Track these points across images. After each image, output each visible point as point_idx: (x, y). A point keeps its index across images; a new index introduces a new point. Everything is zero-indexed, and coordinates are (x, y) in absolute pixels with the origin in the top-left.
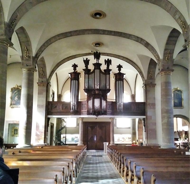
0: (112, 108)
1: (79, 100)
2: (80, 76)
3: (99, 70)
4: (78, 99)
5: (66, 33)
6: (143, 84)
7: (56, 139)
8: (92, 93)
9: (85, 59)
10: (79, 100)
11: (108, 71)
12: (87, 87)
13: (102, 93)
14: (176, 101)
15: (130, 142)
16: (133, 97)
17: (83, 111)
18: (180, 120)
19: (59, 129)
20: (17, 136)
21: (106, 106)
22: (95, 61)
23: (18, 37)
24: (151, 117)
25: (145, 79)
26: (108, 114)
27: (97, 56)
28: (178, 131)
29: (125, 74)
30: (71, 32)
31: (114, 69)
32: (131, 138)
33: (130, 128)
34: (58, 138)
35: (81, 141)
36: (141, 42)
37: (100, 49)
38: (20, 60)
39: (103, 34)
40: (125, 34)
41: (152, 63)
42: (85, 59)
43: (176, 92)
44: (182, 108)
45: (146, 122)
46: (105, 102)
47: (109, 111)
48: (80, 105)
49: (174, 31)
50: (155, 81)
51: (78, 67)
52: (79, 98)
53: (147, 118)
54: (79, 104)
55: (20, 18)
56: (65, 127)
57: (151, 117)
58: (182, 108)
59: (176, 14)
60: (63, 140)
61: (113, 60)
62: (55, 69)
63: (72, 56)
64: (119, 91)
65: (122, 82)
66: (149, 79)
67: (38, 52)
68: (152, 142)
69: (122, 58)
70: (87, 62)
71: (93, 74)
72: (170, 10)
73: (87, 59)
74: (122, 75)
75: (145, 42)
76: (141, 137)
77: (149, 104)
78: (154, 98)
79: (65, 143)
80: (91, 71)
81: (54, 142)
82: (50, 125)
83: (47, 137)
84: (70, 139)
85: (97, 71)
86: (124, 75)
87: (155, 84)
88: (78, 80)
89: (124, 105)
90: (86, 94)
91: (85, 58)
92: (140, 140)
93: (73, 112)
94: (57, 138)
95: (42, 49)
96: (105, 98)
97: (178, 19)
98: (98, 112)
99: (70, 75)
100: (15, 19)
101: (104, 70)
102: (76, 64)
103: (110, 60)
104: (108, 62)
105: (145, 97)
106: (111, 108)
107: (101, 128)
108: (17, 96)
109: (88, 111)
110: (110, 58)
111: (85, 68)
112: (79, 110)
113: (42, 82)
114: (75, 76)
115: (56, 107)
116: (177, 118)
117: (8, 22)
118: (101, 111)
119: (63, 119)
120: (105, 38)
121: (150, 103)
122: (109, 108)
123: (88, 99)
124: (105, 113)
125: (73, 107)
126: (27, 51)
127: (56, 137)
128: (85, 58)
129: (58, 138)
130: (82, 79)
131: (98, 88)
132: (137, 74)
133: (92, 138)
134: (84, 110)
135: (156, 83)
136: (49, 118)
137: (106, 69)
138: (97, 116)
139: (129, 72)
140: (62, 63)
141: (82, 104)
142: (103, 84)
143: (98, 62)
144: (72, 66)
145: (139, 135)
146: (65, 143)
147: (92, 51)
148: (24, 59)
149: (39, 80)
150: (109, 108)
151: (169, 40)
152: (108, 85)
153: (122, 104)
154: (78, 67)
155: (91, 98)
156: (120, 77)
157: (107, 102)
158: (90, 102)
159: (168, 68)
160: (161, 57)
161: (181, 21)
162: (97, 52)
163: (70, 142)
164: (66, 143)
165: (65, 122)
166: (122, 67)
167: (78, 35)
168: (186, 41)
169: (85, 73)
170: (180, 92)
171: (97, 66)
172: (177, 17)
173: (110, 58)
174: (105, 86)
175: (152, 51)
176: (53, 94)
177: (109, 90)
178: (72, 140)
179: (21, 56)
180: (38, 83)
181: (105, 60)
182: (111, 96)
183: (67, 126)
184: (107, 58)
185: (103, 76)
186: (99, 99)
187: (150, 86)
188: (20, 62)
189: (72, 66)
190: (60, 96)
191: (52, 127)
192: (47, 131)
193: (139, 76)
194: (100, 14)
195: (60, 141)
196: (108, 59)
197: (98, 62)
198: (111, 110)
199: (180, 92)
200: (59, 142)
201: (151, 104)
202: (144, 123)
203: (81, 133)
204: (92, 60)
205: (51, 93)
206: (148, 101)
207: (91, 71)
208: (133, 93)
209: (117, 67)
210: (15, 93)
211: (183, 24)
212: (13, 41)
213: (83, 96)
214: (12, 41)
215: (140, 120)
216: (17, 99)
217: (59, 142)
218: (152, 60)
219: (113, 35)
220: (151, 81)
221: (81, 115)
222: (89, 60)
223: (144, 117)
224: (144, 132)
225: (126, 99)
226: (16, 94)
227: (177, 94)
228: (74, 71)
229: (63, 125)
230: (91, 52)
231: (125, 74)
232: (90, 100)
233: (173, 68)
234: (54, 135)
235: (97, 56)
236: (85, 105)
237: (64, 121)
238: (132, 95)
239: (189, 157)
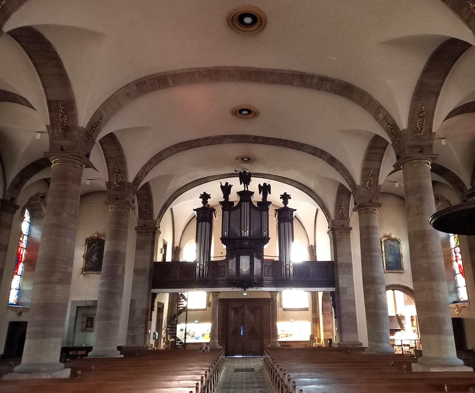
0: (272, 272)
1: (212, 259)
2: (214, 215)
3: (248, 203)
4: (210, 257)
5: (190, 142)
6: (329, 228)
7: (167, 334)
9: (224, 185)
10: (212, 259)
11: (264, 205)
13: (256, 244)
14: (390, 259)
16: (312, 250)
18: (400, 295)
19: (174, 314)
20: (90, 331)
21: (262, 269)
22: (241, 188)
23: (103, 150)
24: (345, 289)
25: (332, 219)
26: (266, 284)
27: (245, 178)
28: (397, 315)
29: (295, 210)
30: (198, 140)
31: (275, 197)
33: (307, 309)
34: (171, 332)
36: (321, 155)
37: (249, 168)
38: (103, 186)
39: (256, 142)
40: (292, 142)
41: (342, 193)
42: (224, 185)
43: (389, 241)
44: (402, 271)
45: (336, 299)
47: (267, 279)
49: (376, 138)
50: (348, 223)
51: (210, 198)
52: (212, 254)
55: (107, 120)
56: (185, 309)
57: (345, 289)
58: (402, 271)
59: (379, 112)
60: (180, 335)
61: (273, 184)
62: (169, 203)
63: (200, 179)
64: (285, 238)
65: (290, 224)
66: (338, 219)
67: (140, 175)
68: (348, 339)
69: (289, 182)
70: (226, 189)
71: (238, 211)
72: (368, 105)
73: (227, 183)
74: (289, 212)
75: (329, 156)
76: (329, 327)
78: (350, 254)
79: (185, 341)
80: (235, 205)
81: (162, 340)
82: (156, 308)
83: (150, 331)
85: (246, 205)
86: (294, 212)
87: (351, 229)
88: (210, 221)
89: (296, 267)
90: (225, 247)
91: (223, 182)
94: (168, 332)
95: (147, 170)
96: (260, 254)
97: (382, 120)
99: (195, 212)
100: (99, 122)
101: (259, 203)
102: (208, 193)
103: (267, 184)
104: (265, 189)
105: (333, 254)
106: (270, 272)
107: (253, 310)
108: (96, 253)
110: (267, 181)
111: (223, 200)
113: (145, 226)
114: (204, 215)
116: (393, 290)
117: (85, 128)
119: (182, 295)
120: (259, 150)
121: (343, 263)
122: (267, 274)
124: (260, 283)
126: (119, 173)
127: (168, 329)
128: (223, 182)
129: (171, 332)
130: (217, 220)
131: (248, 235)
132: (317, 209)
133: (237, 331)
136: (155, 293)
137: (261, 200)
139: (303, 206)
142: (256, 228)
143: (246, 189)
144: (200, 198)
145: (324, 325)
146: (184, 342)
147: (235, 171)
148: (113, 187)
149: (138, 222)
150: (267, 274)
151: (370, 153)
153: (291, 265)
154: (210, 198)
156: (286, 215)
157: (263, 261)
158: (232, 262)
159: (370, 201)
160: (358, 181)
161: (388, 124)
162: (245, 172)
164: (187, 342)
165: (186, 300)
166: (290, 198)
167: (211, 144)
168: (398, 157)
169: (222, 209)
170: (396, 242)
171: (245, 195)
172: (381, 116)
173: (267, 181)
175: (341, 172)
176: (165, 246)
177: (266, 240)
179: (106, 183)
180: (136, 229)
181: (260, 184)
182: (271, 250)
183: (189, 307)
184: (262, 181)
185: (256, 214)
186: (248, 257)
187: (341, 232)
188: (105, 190)
189: (200, 198)
190: (177, 251)
191: (160, 310)
192: (151, 320)
193: (321, 214)
194: (250, 111)
195: (175, 337)
196: (265, 184)
197: (246, 189)
199: (396, 242)
200: (174, 340)
201: (344, 265)
202: (333, 300)
204: (237, 186)
205: (160, 246)
206: (339, 259)
207: (235, 205)
208: (312, 243)
209: (281, 198)
210: (94, 248)
211: (391, 129)
212: (92, 159)
213: (218, 251)
214: (90, 160)
215: (324, 293)
216: (95, 260)
217: (174, 340)
218: (341, 186)
219: (273, 145)
220: (342, 222)
222: (231, 186)
224: (334, 319)
225: (298, 255)
226: (95, 249)
227: (390, 246)
228: (203, 206)
229: (181, 306)
230: (234, 172)
231: (295, 210)
233: (380, 201)
234: (163, 327)
235: (245, 178)
237: (184, 298)
238: (309, 247)
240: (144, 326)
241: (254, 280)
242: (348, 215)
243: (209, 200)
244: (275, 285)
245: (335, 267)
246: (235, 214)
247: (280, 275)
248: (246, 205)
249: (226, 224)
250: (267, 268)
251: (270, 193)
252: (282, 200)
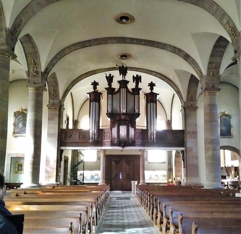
0: (141, 137)
1: (101, 128)
2: (101, 97)
3: (125, 89)
4: (99, 126)
5: (84, 42)
6: (182, 107)
7: (71, 177)
8: (116, 118)
9: (108, 76)
10: (101, 128)
11: (137, 91)
12: (110, 110)
13: (130, 119)
14: (224, 129)
15: (165, 180)
16: (169, 123)
17: (105, 141)
18: (228, 153)
19: (75, 164)
20: (21, 173)
21: (135, 134)
22: (120, 78)
23: (23, 47)
24: (192, 148)
25: (184, 101)
26: (137, 145)
27: (123, 71)
28: (225, 167)
29: (158, 94)
30: (90, 41)
31: (144, 87)
32: (166, 176)
33: (164, 163)
34: (74, 176)
35: (103, 179)
36: (179, 53)
37: (127, 63)
38: (25, 76)
39: (131, 43)
40: (158, 43)
41: (193, 81)
42: (108, 76)
43: (224, 116)
44: (231, 137)
45: (185, 155)
46: (133, 129)
47: (138, 141)
48: (102, 133)
49: (221, 39)
50: (196, 103)
51: (98, 85)
52: (101, 125)
53: (186, 150)
54: (100, 132)
55: (25, 23)
56: (82, 161)
57: (192, 148)
58: (231, 137)
59: (224, 18)
60: (79, 178)
61: (144, 76)
62: (70, 88)
63: (92, 71)
64: (151, 116)
65: (155, 104)
66: (188, 101)
67: (49, 67)
68: (193, 181)
69: (155, 74)
70: (110, 79)
71: (118, 94)
72: (216, 12)
73: (110, 75)
74: (154, 96)
75: (184, 53)
76: (179, 174)
77: (189, 132)
78: (196, 125)
79: (83, 182)
80: (116, 90)
81: (68, 180)
82: (63, 160)
83: (60, 174)
84: (89, 177)
85: (123, 91)
86: (158, 96)
87: (197, 107)
88: (99, 101)
89: (158, 133)
90: (109, 119)
91: (108, 73)
92: (178, 178)
93: (92, 142)
94: (72, 176)
95: (54, 63)
96: (133, 125)
97: (226, 24)
98: (124, 142)
99: (88, 95)
100: (20, 25)
101: (132, 89)
102: (97, 81)
103: (139, 76)
104: (137, 79)
105: (184, 123)
106: (140, 137)
107: (128, 163)
108: (22, 122)
109: (111, 141)
110: (139, 74)
111: (108, 86)
112: (100, 140)
113: (54, 104)
114: (95, 97)
115: (71, 136)
116: (224, 149)
117: (10, 28)
118: (128, 142)
119: (80, 152)
120: (133, 49)
121: (191, 131)
122: (138, 138)
123: (112, 126)
124: (133, 144)
125: (93, 136)
126: (35, 65)
127: (72, 174)
128: (108, 73)
129: (74, 176)
130: (104, 101)
131: (125, 112)
132: (174, 94)
133: (117, 175)
134: (107, 140)
135: (197, 106)
136: (63, 150)
137: (135, 87)
138: (123, 148)
139: (164, 91)
140: (79, 80)
141: (104, 133)
142: (130, 107)
143: (124, 79)
144: (92, 85)
145: (176, 172)
146: (82, 182)
147: (116, 65)
148: (31, 75)
149: (49, 102)
150: (138, 138)
151: (214, 51)
152: (137, 108)
153: (155, 132)
154: (98, 85)
155: (115, 124)
156: (152, 98)
157: (135, 129)
158: (115, 130)
159: (213, 87)
160: (204, 72)
161: (230, 27)
162: (123, 66)
163: (89, 180)
164: (84, 182)
165: (83, 155)
166: (155, 86)
167: (99, 44)
168: (236, 52)
169: (107, 93)
170: (228, 116)
171: (123, 84)
172: (225, 21)
173: (139, 74)
174: (133, 109)
175: (193, 65)
176: (68, 119)
177: (138, 115)
178: (91, 178)
179: (26, 71)
180: (48, 106)
181: (133, 76)
182: (141, 122)
183: (85, 160)
184: (135, 73)
185: (131, 97)
186: (126, 127)
187: (191, 110)
188: (25, 79)
189: (92, 85)
190: (76, 123)
191: (66, 161)
192: (60, 167)
193: (177, 97)
194: (127, 18)
195: (76, 179)
196: (137, 75)
197: (124, 79)
198: (140, 140)
199: (228, 116)
200: (75, 181)
201: (191, 133)
202: (183, 156)
203: (102, 169)
204: (117, 76)
205: (65, 119)
206: (188, 128)
207: (116, 90)
208: (169, 118)
209: (148, 86)
210: (20, 118)
211: (232, 30)
212: (16, 52)
213: (105, 122)
214: (15, 53)
215: (177, 153)
216: (21, 127)
217: (75, 181)
218: (192, 76)
219: (143, 45)
220: (191, 103)
221: (103, 146)
222: (113, 77)
223: (183, 149)
224: (183, 168)
225: (160, 125)
226: (20, 120)
227: (224, 119)
228: (94, 90)
229: (79, 159)
230: (115, 66)
231: (158, 94)
232: (114, 127)
233: (220, 87)
234: (68, 172)
235: (123, 71)
236: (108, 134)
237: (81, 154)
238: (167, 121)
239: (239, 200)
240: (57, 112)
247: (145, 138)
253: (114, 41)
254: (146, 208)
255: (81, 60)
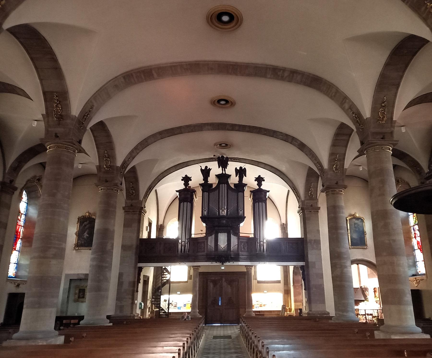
0: (248, 248)
1: (193, 236)
2: (194, 196)
3: (226, 185)
4: (191, 234)
5: (172, 129)
6: (299, 208)
7: (152, 304)
9: (203, 168)
10: (193, 236)
11: (240, 186)
13: (233, 222)
14: (355, 236)
16: (284, 227)
18: (363, 268)
19: (158, 286)
20: (82, 302)
21: (238, 245)
22: (219, 171)
23: (94, 136)
24: (314, 263)
25: (302, 199)
26: (242, 259)
27: (223, 162)
28: (361, 287)
29: (268, 191)
30: (180, 128)
31: (250, 180)
33: (279, 282)
34: (156, 303)
36: (292, 141)
37: (227, 153)
39: (233, 130)
40: (266, 130)
41: (311, 176)
42: (203, 168)
43: (354, 220)
44: (365, 247)
45: (305, 273)
47: (243, 254)
49: (342, 126)
50: (317, 203)
51: (191, 180)
52: (193, 232)
55: (98, 109)
56: (168, 281)
57: (314, 263)
58: (365, 247)
59: (345, 102)
60: (163, 305)
61: (249, 168)
62: (154, 185)
63: (182, 163)
64: (259, 217)
65: (264, 204)
66: (307, 200)
67: (127, 160)
68: (317, 308)
69: (263, 166)
70: (206, 172)
71: (217, 192)
72: (334, 96)
73: (206, 167)
74: (263, 193)
75: (299, 142)
76: (300, 298)
78: (318, 231)
79: (168, 311)
80: (214, 186)
81: (148, 309)
82: (142, 281)
83: (136, 301)
85: (224, 187)
86: (268, 194)
87: (319, 208)
88: (191, 201)
89: (269, 243)
90: (204, 225)
91: (203, 166)
94: (153, 302)
95: (134, 154)
96: (236, 232)
97: (348, 109)
99: (178, 193)
100: (90, 111)
101: (235, 185)
102: (189, 176)
103: (243, 168)
104: (241, 172)
105: (303, 231)
106: (246, 248)
107: (230, 282)
108: (88, 230)
110: (243, 165)
111: (203, 182)
113: (132, 205)
114: (186, 196)
116: (358, 264)
117: (77, 116)
119: (165, 268)
120: (236, 137)
121: (312, 240)
122: (243, 250)
124: (236, 258)
126: (108, 157)
127: (153, 300)
128: (203, 166)
129: (156, 303)
130: (198, 201)
131: (225, 214)
132: (289, 191)
133: (215, 302)
136: (141, 267)
137: (238, 182)
139: (275, 188)
142: (232, 208)
143: (224, 173)
144: (182, 180)
145: (295, 296)
146: (167, 311)
147: (214, 156)
148: (103, 170)
149: (126, 203)
150: (243, 250)
151: (337, 140)
153: (265, 241)
154: (191, 180)
156: (260, 196)
157: (239, 237)
158: (211, 239)
159: (337, 183)
160: (326, 165)
161: (353, 113)
162: (223, 157)
164: (170, 311)
165: (169, 273)
166: (264, 180)
167: (192, 131)
168: (362, 143)
169: (202, 190)
170: (360, 220)
171: (223, 178)
172: (347, 106)
173: (243, 165)
175: (310, 156)
176: (150, 224)
177: (242, 218)
179: (97, 166)
180: (124, 208)
181: (236, 168)
182: (247, 228)
183: (172, 280)
184: (238, 165)
185: (233, 195)
186: (226, 234)
187: (311, 212)
188: (95, 173)
189: (182, 180)
190: (161, 229)
191: (146, 282)
192: (137, 291)
193: (292, 195)
194: (227, 102)
195: (159, 307)
196: (241, 168)
197: (224, 173)
199: (360, 220)
200: (158, 310)
201: (313, 242)
202: (303, 274)
204: (215, 169)
205: (146, 224)
206: (308, 236)
207: (214, 186)
208: (284, 221)
209: (255, 180)
210: (85, 226)
211: (356, 117)
212: (84, 145)
213: (198, 228)
214: (82, 146)
215: (295, 267)
216: (87, 237)
217: (158, 310)
218: (310, 169)
219: (248, 132)
220: (311, 202)
222: (210, 170)
224: (304, 291)
225: (271, 232)
226: (86, 227)
227: (355, 224)
228: (184, 187)
229: (164, 279)
230: (213, 157)
231: (268, 191)
233: (346, 183)
234: (148, 298)
235: (223, 162)
237: (167, 271)
238: (281, 225)
241: (231, 255)
242: (317, 196)
243: (190, 182)
244: (250, 260)
245: (305, 243)
246: (214, 195)
248: (224, 187)
249: (206, 204)
250: (242, 244)
251: (246, 176)
252: (256, 182)
253: (209, 127)
254: (252, 355)
255: (166, 152)
